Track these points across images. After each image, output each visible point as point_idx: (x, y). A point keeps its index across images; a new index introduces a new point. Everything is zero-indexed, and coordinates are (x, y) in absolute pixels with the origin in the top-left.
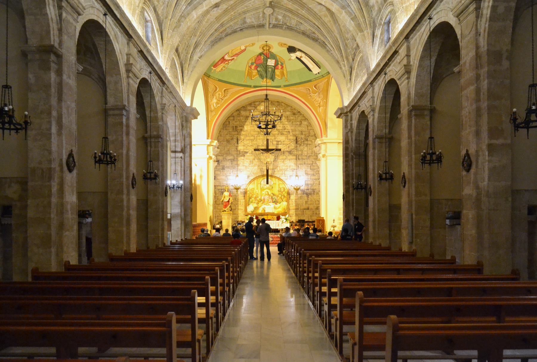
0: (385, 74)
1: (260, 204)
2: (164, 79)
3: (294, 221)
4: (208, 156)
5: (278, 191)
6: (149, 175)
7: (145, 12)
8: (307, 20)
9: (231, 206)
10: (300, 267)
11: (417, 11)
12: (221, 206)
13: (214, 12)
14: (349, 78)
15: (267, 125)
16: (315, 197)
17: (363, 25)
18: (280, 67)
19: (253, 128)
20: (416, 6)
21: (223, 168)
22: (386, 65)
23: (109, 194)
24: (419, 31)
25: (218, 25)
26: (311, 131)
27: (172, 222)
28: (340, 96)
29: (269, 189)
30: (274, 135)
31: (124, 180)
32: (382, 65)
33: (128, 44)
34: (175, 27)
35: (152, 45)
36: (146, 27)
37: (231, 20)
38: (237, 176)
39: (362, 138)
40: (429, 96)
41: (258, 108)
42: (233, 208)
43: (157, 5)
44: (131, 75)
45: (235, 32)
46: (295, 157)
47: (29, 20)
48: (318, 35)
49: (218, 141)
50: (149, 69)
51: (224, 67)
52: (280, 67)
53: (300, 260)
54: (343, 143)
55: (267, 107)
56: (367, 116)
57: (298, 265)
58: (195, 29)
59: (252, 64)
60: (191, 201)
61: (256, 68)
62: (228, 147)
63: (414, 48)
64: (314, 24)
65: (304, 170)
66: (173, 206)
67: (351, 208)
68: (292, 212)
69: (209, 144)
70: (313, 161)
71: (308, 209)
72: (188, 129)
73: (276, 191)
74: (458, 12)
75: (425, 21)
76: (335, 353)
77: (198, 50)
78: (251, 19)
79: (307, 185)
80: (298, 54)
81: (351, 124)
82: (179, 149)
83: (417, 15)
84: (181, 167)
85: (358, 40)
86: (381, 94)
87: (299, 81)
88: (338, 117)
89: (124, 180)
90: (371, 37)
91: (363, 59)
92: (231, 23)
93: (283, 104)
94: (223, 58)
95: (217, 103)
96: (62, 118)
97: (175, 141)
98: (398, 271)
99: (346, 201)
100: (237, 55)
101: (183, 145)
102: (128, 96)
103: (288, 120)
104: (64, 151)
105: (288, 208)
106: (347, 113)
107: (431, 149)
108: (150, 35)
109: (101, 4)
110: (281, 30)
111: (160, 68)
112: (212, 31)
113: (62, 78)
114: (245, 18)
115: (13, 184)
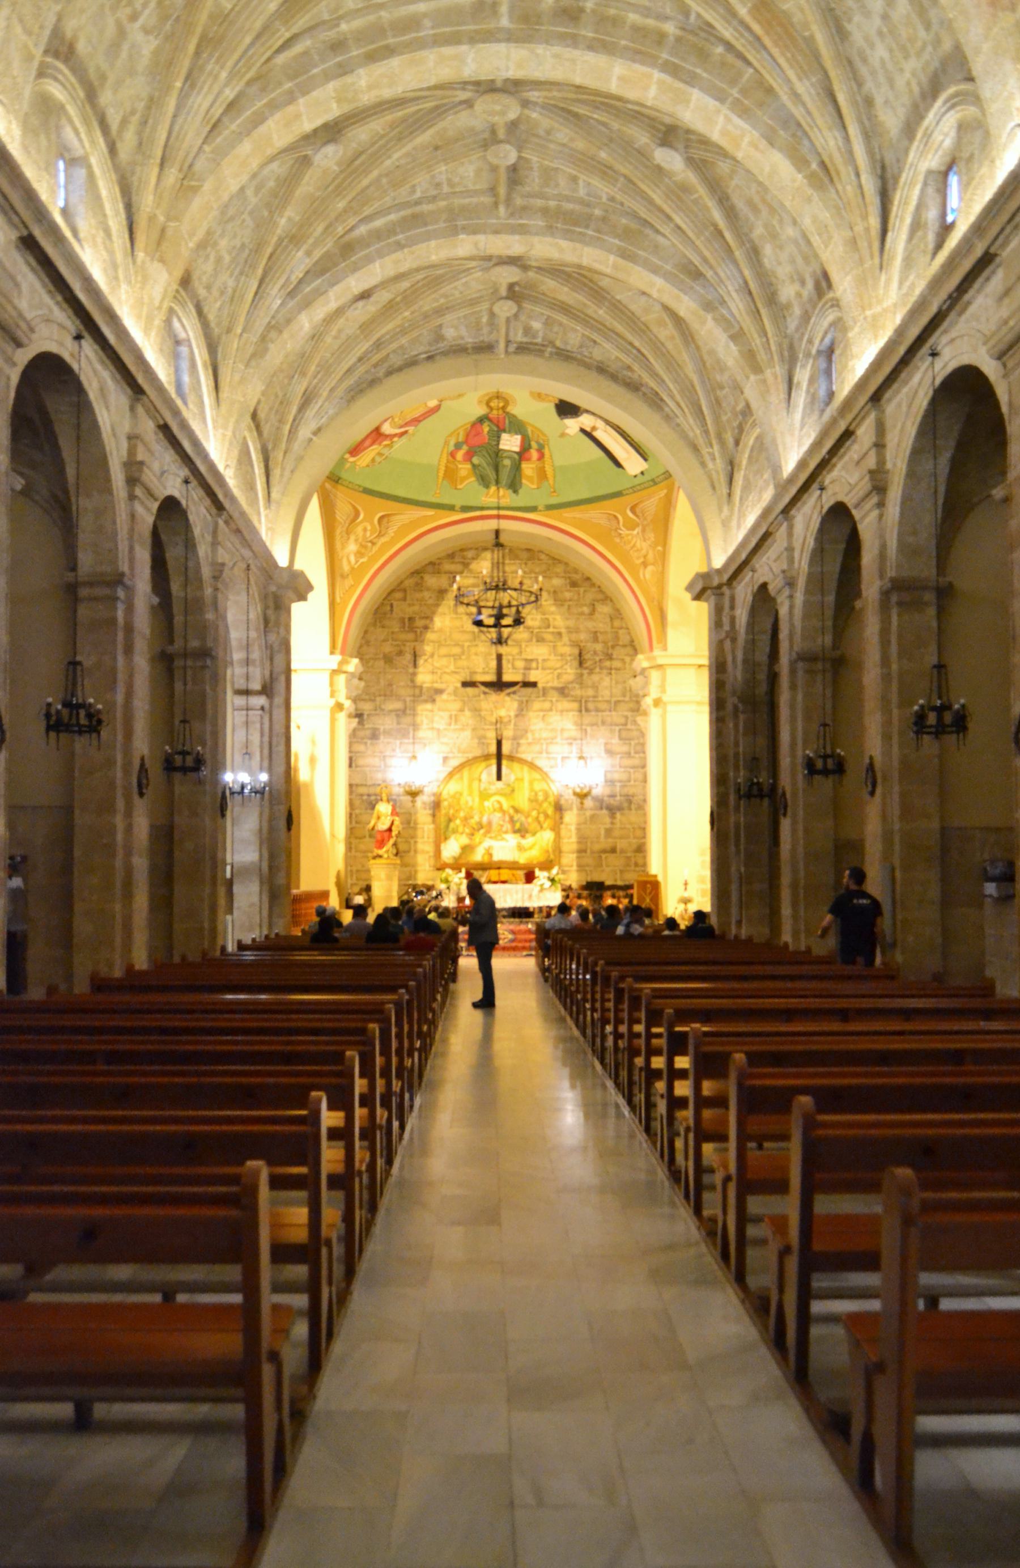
0: (822, 489)
1: (478, 837)
2: (221, 497)
3: (574, 886)
4: (332, 702)
5: (531, 801)
6: (178, 760)
9: (398, 842)
10: (593, 1010)
11: (900, 332)
12: (369, 843)
13: (357, 312)
14: (725, 491)
15: (499, 617)
16: (633, 817)
17: (762, 356)
19: (458, 623)
20: (898, 320)
21: (374, 736)
22: (824, 465)
24: (906, 382)
26: (621, 632)
27: (236, 889)
28: (700, 538)
29: (504, 795)
30: (518, 644)
32: (812, 465)
33: (132, 409)
34: (253, 356)
35: (191, 406)
36: (176, 356)
37: (403, 331)
38: (414, 757)
39: (762, 656)
40: (934, 554)
41: (474, 566)
42: (402, 847)
43: (206, 299)
44: (138, 491)
45: (412, 363)
46: (575, 705)
48: (640, 373)
49: (361, 659)
50: (185, 472)
51: (380, 454)
52: (534, 454)
53: (593, 993)
54: (710, 667)
55: (497, 565)
56: (773, 600)
57: (588, 1006)
59: (458, 446)
60: (289, 829)
61: (469, 456)
63: (895, 426)
64: (631, 344)
65: (602, 741)
66: (242, 845)
67: (733, 849)
68: (569, 859)
69: (335, 667)
70: (627, 717)
71: (613, 850)
72: (282, 631)
73: (522, 800)
74: (1002, 346)
75: (922, 359)
76: (684, 1213)
77: (310, 413)
78: (456, 328)
79: (610, 782)
80: (585, 421)
81: (733, 620)
82: (256, 686)
83: (900, 343)
84: (262, 735)
85: (751, 392)
86: (811, 543)
87: (586, 495)
88: (697, 597)
89: (119, 774)
90: (783, 387)
91: (762, 443)
92: (404, 341)
93: (543, 557)
95: (359, 554)
97: (247, 662)
98: (844, 1015)
99: (718, 830)
100: (416, 421)
101: (267, 673)
102: (131, 549)
103: (559, 601)
105: (558, 850)
106: (720, 586)
107: (940, 698)
108: (186, 379)
110: (539, 361)
111: (212, 467)
114: (440, 326)
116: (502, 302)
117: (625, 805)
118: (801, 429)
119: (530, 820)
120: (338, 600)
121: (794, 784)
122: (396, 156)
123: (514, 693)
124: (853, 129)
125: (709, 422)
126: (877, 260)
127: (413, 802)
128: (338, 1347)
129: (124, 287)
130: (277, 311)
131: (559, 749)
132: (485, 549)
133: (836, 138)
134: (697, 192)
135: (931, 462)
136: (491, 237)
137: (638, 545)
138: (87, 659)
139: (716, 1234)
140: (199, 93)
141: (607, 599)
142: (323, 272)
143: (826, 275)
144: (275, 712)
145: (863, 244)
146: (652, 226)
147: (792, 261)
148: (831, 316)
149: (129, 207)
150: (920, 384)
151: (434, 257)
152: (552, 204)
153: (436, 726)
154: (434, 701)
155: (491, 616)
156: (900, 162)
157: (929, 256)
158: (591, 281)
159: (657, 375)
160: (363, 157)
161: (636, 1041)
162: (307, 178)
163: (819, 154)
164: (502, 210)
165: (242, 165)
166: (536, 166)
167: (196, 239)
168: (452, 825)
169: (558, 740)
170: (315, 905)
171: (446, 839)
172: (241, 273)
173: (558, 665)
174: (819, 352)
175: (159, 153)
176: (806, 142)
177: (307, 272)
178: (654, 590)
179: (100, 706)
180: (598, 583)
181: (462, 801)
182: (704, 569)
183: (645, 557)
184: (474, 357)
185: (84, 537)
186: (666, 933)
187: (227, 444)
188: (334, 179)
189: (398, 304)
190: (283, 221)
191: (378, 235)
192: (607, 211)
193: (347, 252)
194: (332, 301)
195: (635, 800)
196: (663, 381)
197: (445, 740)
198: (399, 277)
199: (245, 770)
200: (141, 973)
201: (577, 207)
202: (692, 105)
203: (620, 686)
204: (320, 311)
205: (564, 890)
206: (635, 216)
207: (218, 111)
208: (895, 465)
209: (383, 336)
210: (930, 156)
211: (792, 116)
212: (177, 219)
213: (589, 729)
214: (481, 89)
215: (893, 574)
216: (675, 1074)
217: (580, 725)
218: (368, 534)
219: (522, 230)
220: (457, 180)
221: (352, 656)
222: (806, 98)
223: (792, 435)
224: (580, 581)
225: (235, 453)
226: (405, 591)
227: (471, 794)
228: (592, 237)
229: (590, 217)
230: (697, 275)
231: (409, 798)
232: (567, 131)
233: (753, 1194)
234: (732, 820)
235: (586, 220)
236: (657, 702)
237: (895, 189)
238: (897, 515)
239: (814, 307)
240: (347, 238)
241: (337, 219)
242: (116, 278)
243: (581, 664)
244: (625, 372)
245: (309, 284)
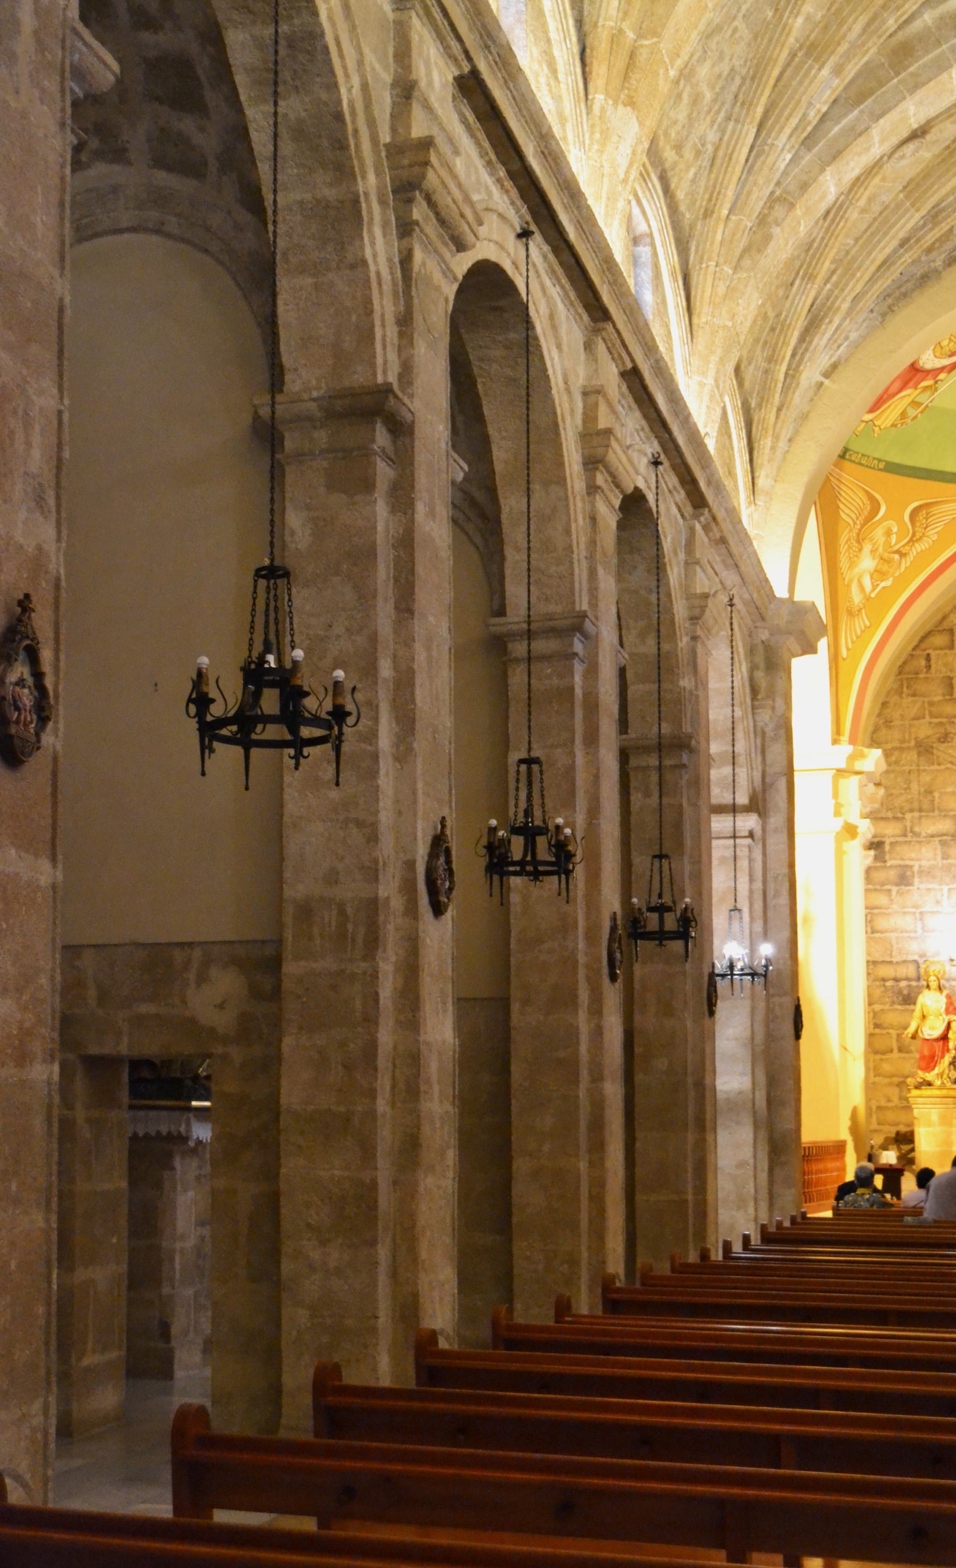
4: (838, 824)
6: (652, 923)
12: (908, 1064)
13: (904, 162)
21: (904, 879)
23: (515, 1007)
25: (918, 216)
31: (581, 945)
33: (589, 346)
34: (747, 250)
43: (675, 164)
47: (291, 292)
51: (915, 404)
60: (798, 1036)
62: (926, 778)
69: (843, 765)
72: (779, 702)
77: (821, 340)
82: (742, 799)
89: (581, 945)
95: (878, 575)
96: (411, 684)
101: (757, 776)
102: (592, 573)
104: (420, 825)
109: (514, 193)
112: (888, 246)
113: (413, 521)
115: (214, 972)
120: (844, 653)
130: (785, 173)
142: (861, 98)
144: (770, 841)
167: (679, 62)
172: (728, 119)
177: (835, 101)
187: (706, 398)
190: (800, 20)
194: (876, 142)
204: (853, 165)
212: (655, 33)
218: (894, 539)
226: (951, 631)
240: (900, 36)
245: (838, 122)
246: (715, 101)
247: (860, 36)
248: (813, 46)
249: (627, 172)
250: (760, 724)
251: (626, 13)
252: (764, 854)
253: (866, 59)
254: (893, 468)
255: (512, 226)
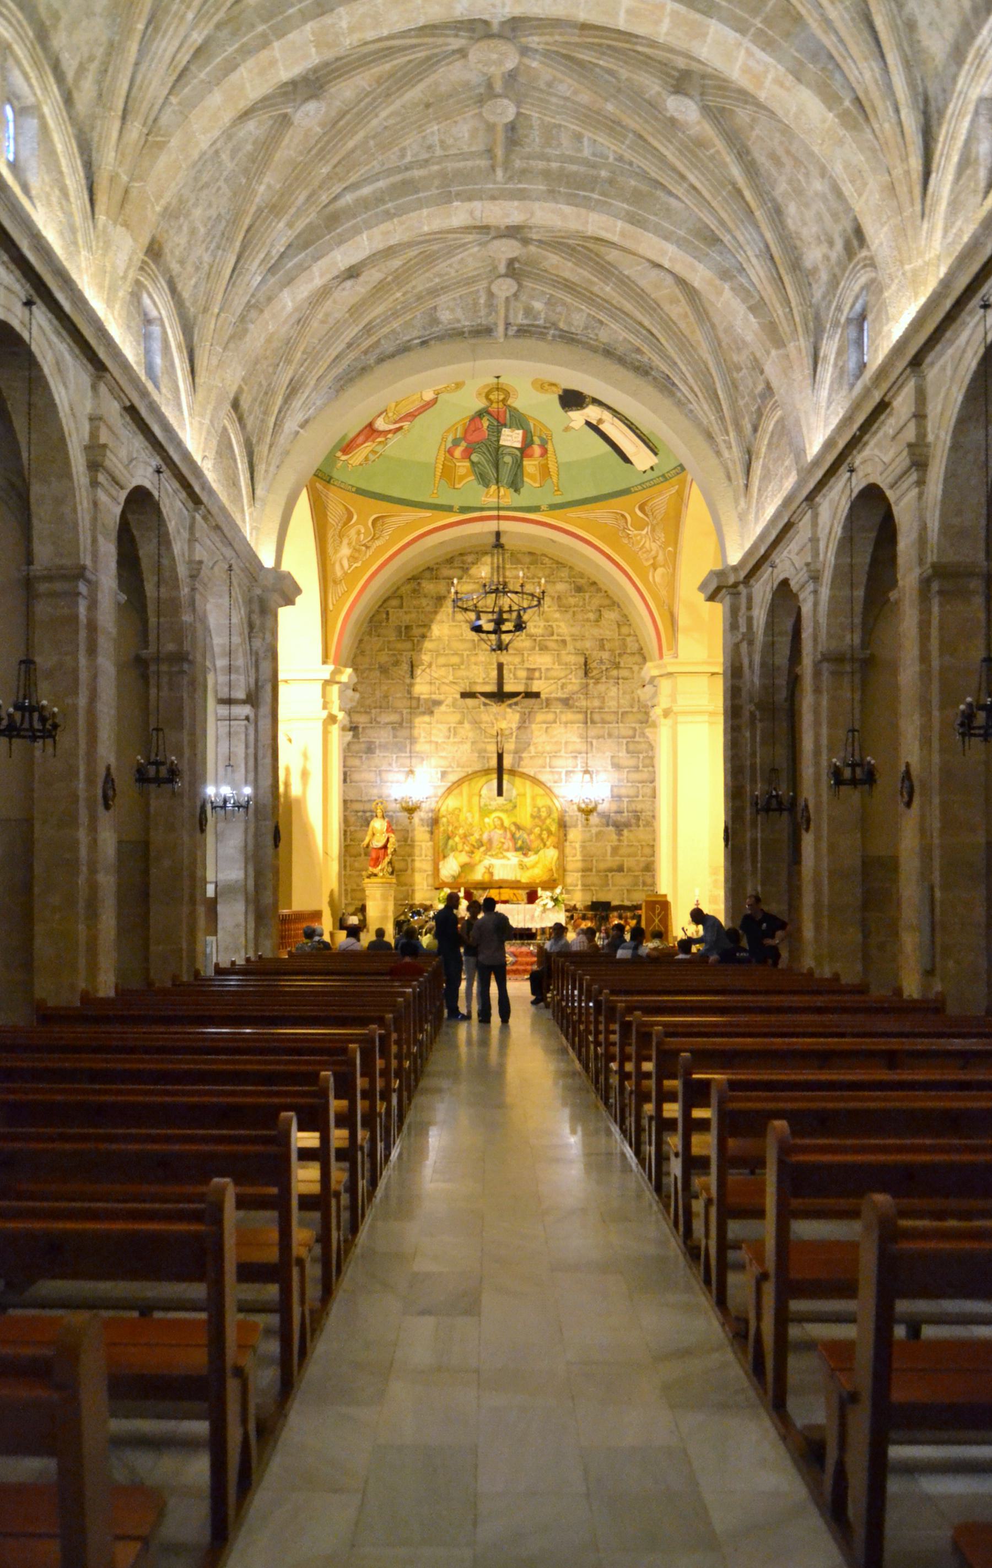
0: (852, 471)
1: (478, 855)
2: (197, 489)
3: (579, 906)
4: (324, 714)
5: (533, 817)
6: (152, 770)
7: (145, 296)
8: (616, 312)
10: (597, 1043)
11: (946, 284)
13: (345, 293)
14: (742, 482)
15: (499, 622)
17: (784, 328)
18: (537, 450)
19: (457, 632)
21: (370, 750)
22: (855, 443)
24: (951, 342)
25: (356, 330)
26: (629, 639)
27: (220, 908)
28: (714, 537)
29: (505, 811)
30: (520, 652)
31: (82, 785)
32: (841, 444)
33: (94, 387)
34: (232, 337)
35: (164, 390)
36: (147, 337)
39: (782, 658)
41: (473, 571)
42: (398, 865)
44: (101, 478)
45: (405, 349)
48: (650, 356)
49: (355, 670)
50: (156, 461)
52: (537, 450)
53: (597, 1023)
54: (725, 674)
55: (498, 569)
56: (796, 596)
57: (591, 1038)
58: (289, 344)
59: (456, 443)
60: (276, 845)
61: (467, 454)
62: (385, 688)
64: (640, 324)
65: (608, 754)
66: (224, 862)
67: (748, 866)
68: (573, 878)
69: (328, 677)
70: (635, 729)
71: (620, 869)
72: (268, 635)
73: (524, 816)
75: (971, 313)
76: (704, 1301)
77: (297, 403)
78: (452, 310)
79: (617, 797)
80: (592, 413)
81: (750, 620)
82: (240, 694)
83: (946, 297)
84: (247, 747)
85: (771, 370)
86: (838, 531)
88: (711, 598)
89: (82, 785)
90: (808, 362)
91: (783, 427)
92: (395, 325)
93: (546, 560)
94: (370, 425)
95: (353, 559)
97: (230, 669)
98: (892, 1059)
100: (411, 416)
101: (252, 681)
102: (94, 541)
103: (563, 607)
105: (562, 868)
106: (735, 585)
108: (158, 360)
109: (18, 273)
110: (542, 344)
111: (187, 456)
112: (340, 346)
114: (435, 308)
116: (500, 280)
117: (633, 821)
118: (828, 408)
119: (532, 837)
120: (331, 607)
121: (818, 795)
122: (383, 114)
123: (516, 704)
124: (892, 58)
125: (725, 407)
126: (918, 208)
127: (410, 818)
128: (261, 1498)
129: (84, 253)
130: (257, 288)
131: (564, 763)
132: (486, 553)
133: (872, 70)
134: (714, 146)
135: (981, 433)
136: (489, 205)
137: (647, 545)
138: (43, 661)
139: (746, 1337)
140: (163, 37)
141: (614, 604)
142: (306, 245)
143: (859, 232)
145: (902, 190)
146: (664, 187)
147: (819, 218)
148: (863, 279)
149: (89, 166)
150: (968, 342)
151: (426, 229)
152: (554, 165)
153: (433, 739)
154: (431, 713)
155: (490, 621)
156: (946, 92)
157: (981, 195)
158: (597, 255)
159: (669, 357)
160: (348, 117)
161: (645, 1082)
162: (286, 141)
163: (853, 89)
164: (500, 173)
165: (210, 119)
166: (536, 123)
167: (163, 202)
168: (451, 842)
169: (562, 753)
170: (305, 925)
171: (445, 857)
172: (218, 247)
173: (562, 674)
174: (849, 320)
175: (120, 105)
176: (837, 76)
177: (290, 246)
178: (663, 593)
179: (56, 709)
180: (604, 588)
181: (462, 817)
182: (719, 567)
183: (655, 558)
184: (473, 341)
185: (40, 527)
186: (681, 956)
187: (204, 434)
188: (317, 142)
189: (389, 284)
191: (365, 204)
192: (613, 172)
193: (332, 223)
194: (318, 276)
195: (643, 816)
196: (675, 363)
197: (444, 754)
198: (389, 252)
199: (229, 784)
200: (106, 1001)
201: (583, 169)
202: (709, 40)
203: (628, 697)
204: (305, 288)
205: (567, 911)
206: (644, 176)
207: (184, 58)
208: (937, 437)
209: (375, 319)
210: (982, 81)
211: (823, 47)
212: (142, 179)
213: (594, 742)
214: (476, 35)
215: (935, 559)
216: (693, 1126)
217: (585, 738)
219: (521, 195)
220: (450, 141)
221: (346, 666)
222: (839, 25)
223: (818, 414)
224: (585, 586)
225: (214, 443)
226: (401, 597)
227: (470, 811)
228: (598, 201)
229: (595, 179)
230: (714, 240)
231: (406, 814)
232: (570, 81)
233: (795, 1298)
234: (748, 835)
235: (590, 183)
236: (666, 713)
237: (940, 125)
238: (940, 492)
239: (844, 270)
241: (320, 187)
242: (75, 243)
243: (586, 674)
244: (633, 355)
246: (208, 234)
247: (304, 204)
248: (274, 206)
249: (126, 272)
250: (254, 648)
251: (121, 162)
252: (256, 731)
253: (308, 220)
254: (360, 492)
255: (18, 296)
